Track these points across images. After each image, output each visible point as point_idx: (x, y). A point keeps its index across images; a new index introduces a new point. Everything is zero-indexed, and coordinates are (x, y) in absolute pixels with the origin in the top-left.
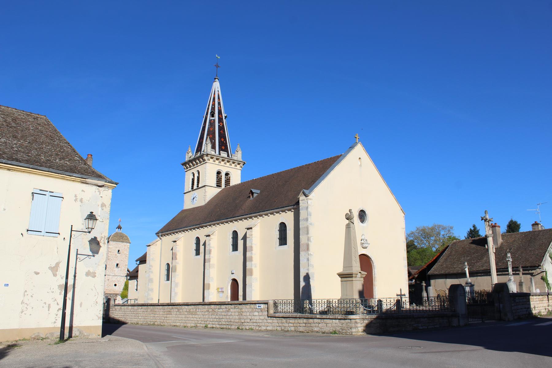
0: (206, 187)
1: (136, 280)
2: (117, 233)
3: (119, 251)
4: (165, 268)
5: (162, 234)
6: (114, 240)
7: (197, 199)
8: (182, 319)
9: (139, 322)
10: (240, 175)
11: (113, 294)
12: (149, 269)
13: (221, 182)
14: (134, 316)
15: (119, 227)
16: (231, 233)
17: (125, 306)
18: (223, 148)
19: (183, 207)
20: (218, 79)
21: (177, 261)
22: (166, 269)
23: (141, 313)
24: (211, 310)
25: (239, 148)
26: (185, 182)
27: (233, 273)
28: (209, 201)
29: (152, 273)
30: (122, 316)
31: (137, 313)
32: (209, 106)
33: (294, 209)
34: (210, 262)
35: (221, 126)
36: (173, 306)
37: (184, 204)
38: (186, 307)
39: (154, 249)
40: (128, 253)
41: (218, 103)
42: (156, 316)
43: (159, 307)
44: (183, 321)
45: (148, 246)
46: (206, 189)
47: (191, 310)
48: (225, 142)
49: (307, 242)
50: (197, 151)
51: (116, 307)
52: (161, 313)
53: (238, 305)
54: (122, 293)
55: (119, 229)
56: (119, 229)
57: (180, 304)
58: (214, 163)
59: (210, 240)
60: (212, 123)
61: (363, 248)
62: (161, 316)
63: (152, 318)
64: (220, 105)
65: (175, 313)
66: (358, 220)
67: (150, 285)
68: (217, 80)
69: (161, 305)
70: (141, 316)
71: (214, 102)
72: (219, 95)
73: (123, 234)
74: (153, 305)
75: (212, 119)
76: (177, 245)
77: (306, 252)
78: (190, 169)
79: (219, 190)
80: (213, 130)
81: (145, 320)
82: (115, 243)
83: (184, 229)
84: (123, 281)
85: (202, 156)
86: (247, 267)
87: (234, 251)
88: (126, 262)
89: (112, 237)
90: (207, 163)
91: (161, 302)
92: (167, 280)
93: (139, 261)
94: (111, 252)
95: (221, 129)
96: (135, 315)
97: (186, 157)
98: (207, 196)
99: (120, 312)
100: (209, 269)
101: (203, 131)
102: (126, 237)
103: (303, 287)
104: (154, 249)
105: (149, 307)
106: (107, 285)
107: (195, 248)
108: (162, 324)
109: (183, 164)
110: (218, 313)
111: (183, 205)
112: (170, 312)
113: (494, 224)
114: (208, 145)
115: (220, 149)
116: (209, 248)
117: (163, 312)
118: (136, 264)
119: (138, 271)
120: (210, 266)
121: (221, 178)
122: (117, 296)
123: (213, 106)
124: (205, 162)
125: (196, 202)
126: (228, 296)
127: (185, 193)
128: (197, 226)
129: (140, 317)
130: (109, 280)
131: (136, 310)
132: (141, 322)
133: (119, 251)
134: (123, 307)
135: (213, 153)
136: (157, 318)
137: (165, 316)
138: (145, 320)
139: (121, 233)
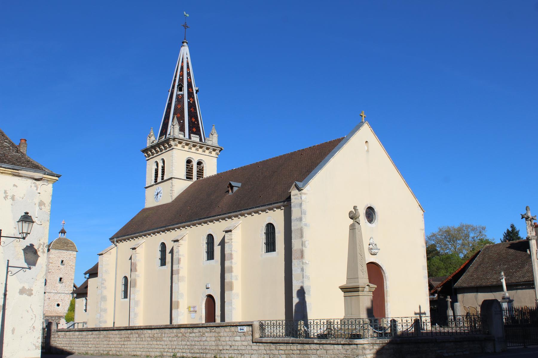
1: (84, 298)
2: (59, 239)
3: (62, 261)
5: (117, 239)
7: (161, 195)
9: (89, 352)
11: (56, 316)
13: (192, 173)
14: (83, 344)
15: (63, 232)
17: (70, 332)
18: (194, 130)
20: (187, 43)
21: (137, 273)
24: (180, 335)
25: (214, 131)
26: (147, 173)
28: (177, 197)
31: (87, 340)
32: (176, 77)
33: (284, 206)
34: (178, 273)
35: (191, 102)
38: (149, 331)
39: (108, 259)
40: (74, 264)
42: (111, 343)
43: (114, 331)
47: (156, 335)
48: (196, 123)
50: (161, 135)
51: (59, 333)
52: (117, 339)
54: (67, 314)
55: (63, 234)
56: (63, 234)
57: (142, 328)
58: (182, 149)
59: (179, 246)
60: (180, 99)
61: (372, 255)
63: (105, 346)
64: (190, 75)
65: (135, 339)
66: (365, 219)
68: (185, 44)
72: (188, 63)
73: (68, 240)
74: (106, 329)
75: (180, 94)
80: (181, 107)
81: (97, 349)
82: (57, 251)
83: (146, 233)
84: (68, 299)
85: (167, 141)
89: (53, 245)
90: (174, 150)
93: (88, 274)
94: (52, 263)
95: (192, 106)
96: (84, 343)
99: (64, 339)
100: (178, 283)
101: (188, 72)
102: (72, 243)
105: (102, 332)
106: (48, 305)
107: (160, 256)
108: (118, 353)
110: (190, 338)
112: (128, 337)
114: (175, 126)
115: (191, 132)
116: (177, 256)
117: (119, 338)
118: (85, 278)
119: (87, 287)
121: (192, 169)
122: (60, 319)
123: (181, 78)
124: (172, 148)
127: (146, 188)
128: (162, 229)
129: (90, 346)
130: (49, 299)
131: (85, 336)
132: (92, 352)
133: (62, 261)
134: (68, 333)
135: (181, 136)
136: (112, 346)
137: (122, 343)
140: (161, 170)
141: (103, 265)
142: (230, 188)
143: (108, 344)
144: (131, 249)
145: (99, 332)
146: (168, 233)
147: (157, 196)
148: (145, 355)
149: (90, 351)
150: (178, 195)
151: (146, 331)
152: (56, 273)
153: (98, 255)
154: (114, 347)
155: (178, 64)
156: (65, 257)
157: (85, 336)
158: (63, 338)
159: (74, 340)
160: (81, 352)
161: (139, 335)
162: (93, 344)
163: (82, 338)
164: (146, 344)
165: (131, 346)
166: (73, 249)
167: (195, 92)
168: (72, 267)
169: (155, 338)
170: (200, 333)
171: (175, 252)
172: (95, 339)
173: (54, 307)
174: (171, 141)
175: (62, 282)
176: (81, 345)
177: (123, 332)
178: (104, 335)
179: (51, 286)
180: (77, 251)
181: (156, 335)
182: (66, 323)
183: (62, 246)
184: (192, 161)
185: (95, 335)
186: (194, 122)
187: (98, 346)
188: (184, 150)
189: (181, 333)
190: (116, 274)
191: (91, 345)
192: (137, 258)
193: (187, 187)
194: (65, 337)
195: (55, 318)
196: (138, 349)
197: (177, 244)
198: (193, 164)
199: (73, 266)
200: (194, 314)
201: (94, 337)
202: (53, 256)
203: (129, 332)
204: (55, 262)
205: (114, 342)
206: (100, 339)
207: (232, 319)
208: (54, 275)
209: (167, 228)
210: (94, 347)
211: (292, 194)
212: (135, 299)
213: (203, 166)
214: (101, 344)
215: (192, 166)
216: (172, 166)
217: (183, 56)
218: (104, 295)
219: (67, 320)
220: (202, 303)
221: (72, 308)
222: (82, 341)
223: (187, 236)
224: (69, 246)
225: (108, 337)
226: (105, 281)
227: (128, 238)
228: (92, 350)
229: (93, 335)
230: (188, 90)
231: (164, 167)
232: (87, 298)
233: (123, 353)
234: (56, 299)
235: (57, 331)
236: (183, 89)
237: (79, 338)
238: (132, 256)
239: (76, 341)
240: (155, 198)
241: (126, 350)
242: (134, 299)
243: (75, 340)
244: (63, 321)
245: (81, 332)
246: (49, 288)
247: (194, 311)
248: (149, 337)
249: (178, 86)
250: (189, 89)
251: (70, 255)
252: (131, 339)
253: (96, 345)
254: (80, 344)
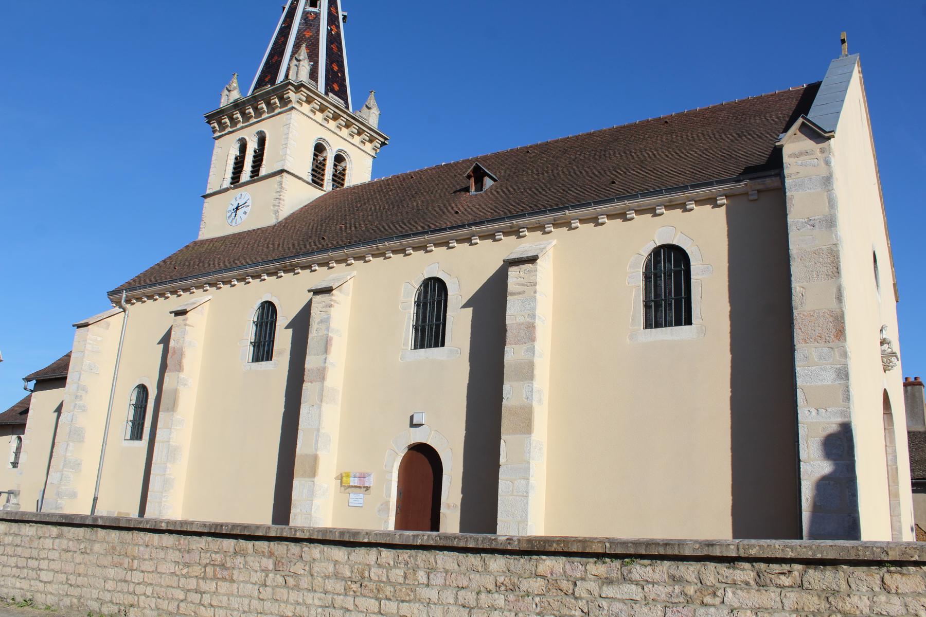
0: (285, 174)
1: (15, 437)
4: (132, 397)
5: (130, 294)
7: (247, 210)
9: (40, 598)
10: (371, 169)
12: (76, 397)
14: (17, 567)
18: (336, 87)
19: (198, 235)
21: (182, 375)
23: (54, 555)
24: (537, 585)
28: (290, 216)
31: (35, 553)
33: (727, 197)
34: (323, 378)
35: (333, 33)
36: (242, 542)
37: (202, 226)
38: (339, 553)
39: (99, 339)
42: (137, 577)
48: (340, 75)
49: (834, 304)
50: (260, 83)
53: (798, 567)
59: (331, 306)
60: (310, 22)
63: (110, 585)
65: (257, 577)
67: (70, 448)
69: (171, 532)
70: (53, 570)
71: (288, 20)
74: (122, 525)
76: (189, 326)
77: (831, 345)
80: (311, 36)
83: (218, 276)
85: (281, 92)
86: (504, 402)
87: (422, 347)
90: (294, 112)
91: (104, 510)
92: (132, 438)
93: (34, 382)
95: (333, 40)
96: (22, 562)
97: (222, 101)
98: (284, 200)
100: (320, 407)
101: (283, 39)
103: (823, 484)
104: (99, 339)
105: (101, 533)
107: (253, 337)
109: (210, 118)
110: (604, 604)
111: (199, 229)
112: (223, 566)
113: (913, 380)
114: (302, 63)
115: (329, 88)
117: (177, 563)
118: (25, 389)
119: (26, 411)
121: (324, 165)
124: (289, 106)
125: (244, 217)
127: (205, 197)
128: (270, 266)
129: (45, 576)
131: (31, 540)
132: (50, 600)
136: (140, 589)
137: (192, 584)
138: (72, 591)
140: (252, 157)
143: (126, 581)
144: (171, 313)
145: (88, 530)
147: (236, 212)
150: (292, 212)
151: (322, 552)
153: (74, 326)
157: (31, 540)
162: (57, 572)
164: (317, 602)
167: (341, 18)
170: (677, 589)
171: (317, 322)
174: (289, 91)
177: (199, 543)
178: (108, 543)
184: (327, 148)
185: (70, 540)
187: (80, 580)
189: (544, 577)
191: (51, 574)
198: (326, 156)
200: (361, 496)
206: (92, 558)
207: (524, 521)
210: (61, 583)
211: (786, 152)
212: (171, 443)
213: (345, 167)
214: (94, 576)
215: (325, 160)
220: (393, 467)
222: (15, 556)
223: (351, 282)
225: (126, 555)
226: (87, 392)
228: (51, 593)
229: (65, 542)
231: (262, 155)
232: (22, 436)
238: (173, 333)
240: (230, 216)
242: (169, 442)
245: (14, 525)
247: (360, 487)
252: (235, 572)
253: (71, 577)
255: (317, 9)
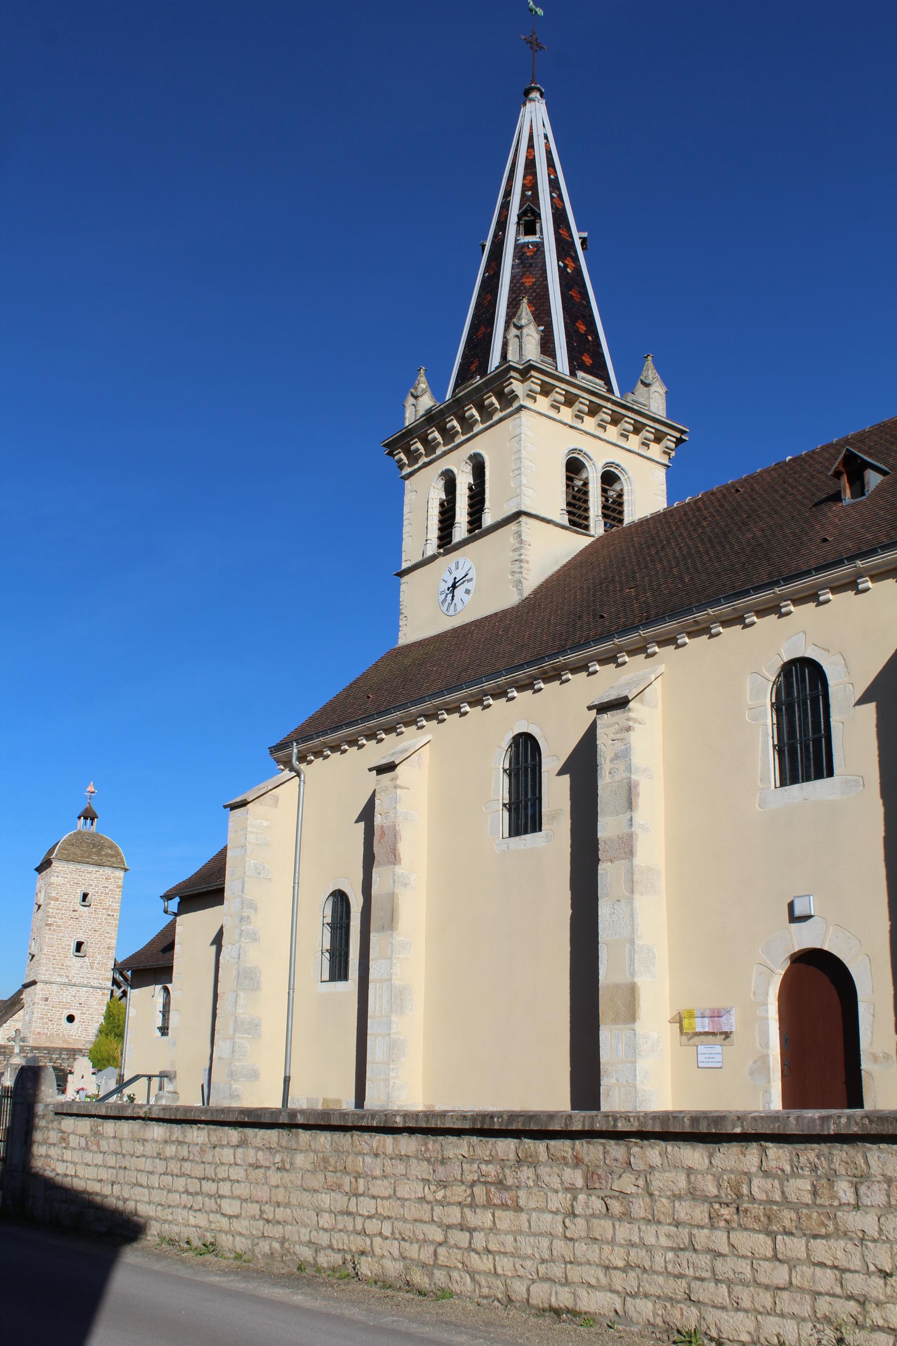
0: (523, 519)
1: (159, 987)
2: (79, 833)
3: (85, 896)
5: (303, 746)
6: (71, 858)
8: (638, 1256)
9: (225, 1241)
10: (664, 487)
11: (62, 1049)
12: (242, 919)
14: (187, 1192)
15: (89, 815)
16: (771, 674)
17: (119, 1123)
18: (587, 360)
21: (399, 870)
22: (329, 920)
23: (237, 1173)
25: (650, 372)
27: (806, 918)
29: (255, 940)
30: (101, 1181)
31: (210, 1171)
35: (569, 270)
39: (265, 824)
40: (116, 906)
41: (550, 181)
42: (366, 1206)
43: (389, 1139)
44: (658, 1284)
45: (234, 807)
46: (524, 527)
47: (759, 1187)
48: (590, 338)
50: (463, 377)
51: (68, 1124)
52: (411, 1189)
54: (94, 1045)
55: (89, 821)
56: (89, 821)
57: (621, 1126)
59: (629, 729)
62: (413, 1211)
63: (326, 1220)
64: (559, 189)
65: (559, 1200)
67: (241, 1001)
73: (102, 837)
74: (334, 1122)
75: (528, 243)
76: (402, 788)
78: (426, 460)
79: (578, 543)
80: (534, 284)
81: (277, 1232)
82: (72, 866)
83: (437, 701)
84: (99, 1004)
87: (794, 781)
88: (110, 938)
89: (62, 848)
90: (524, 413)
93: (177, 900)
94: (57, 900)
96: (194, 1186)
97: (407, 415)
98: (527, 562)
99: (88, 1157)
100: (631, 902)
101: (552, 177)
102: (112, 847)
105: (304, 1136)
106: (42, 1018)
107: (507, 795)
108: (419, 1278)
109: (391, 447)
111: (396, 628)
112: (500, 1184)
114: (525, 331)
115: (575, 365)
116: (621, 775)
117: (426, 1181)
118: (166, 912)
119: (170, 947)
120: (636, 877)
122: (75, 1059)
123: (530, 193)
124: (515, 405)
125: (466, 598)
126: (765, 1058)
127: (402, 574)
130: (47, 1000)
131: (202, 1151)
132: (241, 1244)
133: (85, 896)
134: (109, 1127)
136: (372, 1226)
137: (454, 1215)
138: (270, 1230)
139: (92, 835)
141: (249, 847)
142: (845, 477)
143: (349, 1214)
145: (284, 1132)
146: (550, 689)
148: (659, 1321)
149: (230, 1238)
152: (67, 928)
153: (225, 807)
154: (387, 1231)
155: (516, 150)
156: (91, 885)
157: (202, 1151)
158: (87, 1149)
159: (142, 1168)
160: (179, 1234)
161: (590, 1176)
162: (245, 1200)
163: (183, 1159)
164: (664, 1241)
165: (526, 1246)
166: (116, 864)
168: (112, 914)
169: (757, 1210)
171: (608, 758)
172: (262, 1170)
173: (57, 1025)
174: (512, 380)
175: (82, 955)
176: (175, 1198)
178: (315, 1152)
179: (54, 964)
180: (126, 870)
181: (759, 1187)
182: (93, 1070)
183: (85, 852)
184: (587, 464)
186: (586, 335)
187: (281, 1213)
188: (558, 418)
190: (296, 883)
192: (401, 808)
193: (573, 556)
194: (94, 1148)
195: (60, 1054)
196: (592, 1274)
197: (615, 719)
198: (587, 478)
199: (113, 910)
200: (718, 1049)
201: (252, 1160)
202: (60, 880)
203: (506, 1147)
204: (66, 897)
205: (387, 1203)
208: (62, 934)
209: (547, 665)
210: (253, 1218)
213: (622, 490)
214: (301, 1206)
216: (516, 472)
217: (531, 126)
218: (249, 965)
219: (96, 1061)
220: (767, 994)
221: (110, 1026)
222: (183, 1175)
223: (658, 684)
224: (105, 855)
225: (345, 1171)
227: (351, 735)
228: (241, 1234)
230: (557, 233)
232: (169, 986)
233: (463, 1284)
234: (64, 1000)
235: (57, 1114)
236: (538, 226)
237: (165, 1159)
239: (152, 1173)
241: (483, 1264)
243: (147, 1165)
244: (83, 1066)
245: (177, 1129)
246: (46, 970)
248: (694, 1194)
249: (520, 217)
250: (560, 231)
251: (106, 879)
252: (522, 1194)
253: (266, 1208)
254: (169, 1191)
255: (538, 236)
